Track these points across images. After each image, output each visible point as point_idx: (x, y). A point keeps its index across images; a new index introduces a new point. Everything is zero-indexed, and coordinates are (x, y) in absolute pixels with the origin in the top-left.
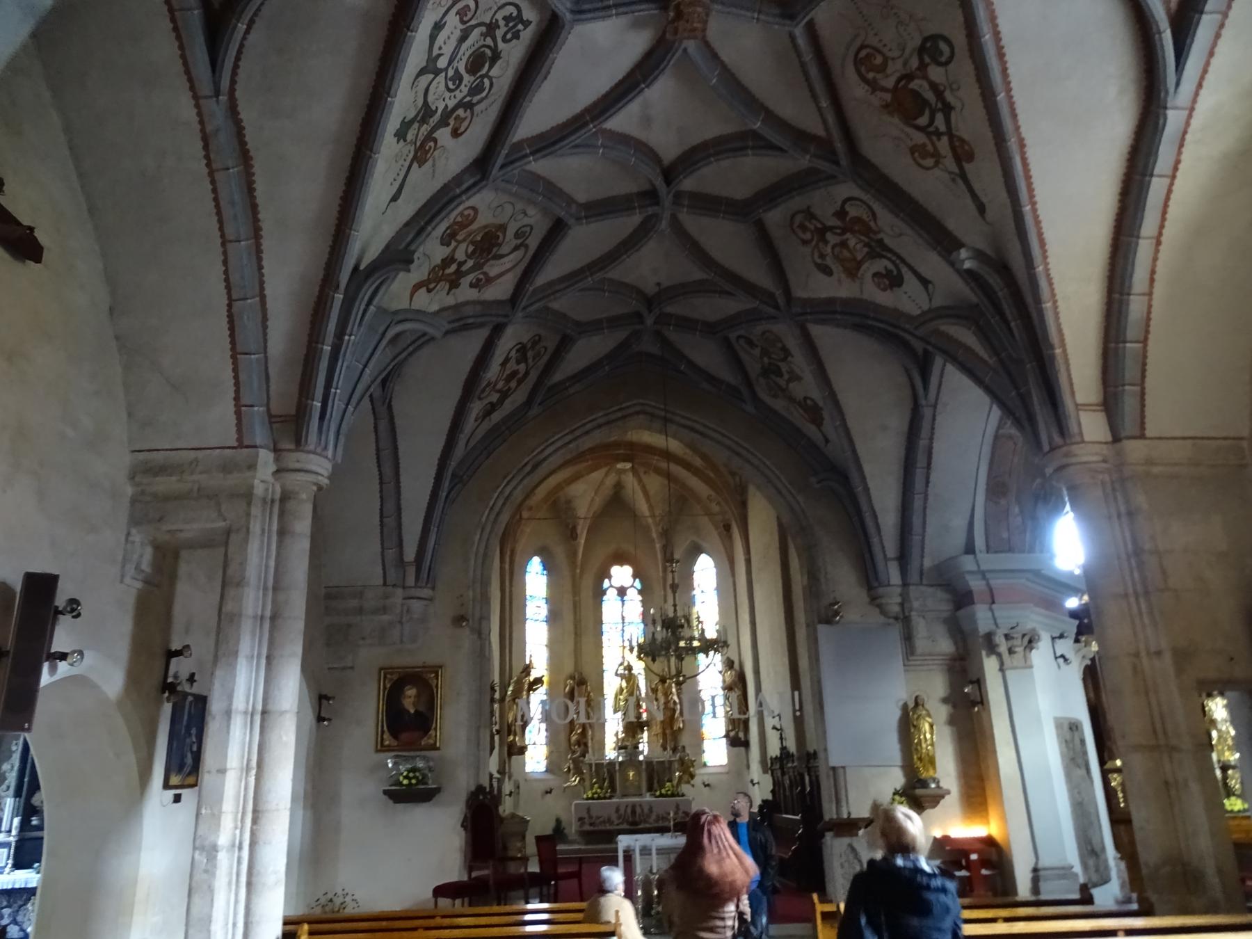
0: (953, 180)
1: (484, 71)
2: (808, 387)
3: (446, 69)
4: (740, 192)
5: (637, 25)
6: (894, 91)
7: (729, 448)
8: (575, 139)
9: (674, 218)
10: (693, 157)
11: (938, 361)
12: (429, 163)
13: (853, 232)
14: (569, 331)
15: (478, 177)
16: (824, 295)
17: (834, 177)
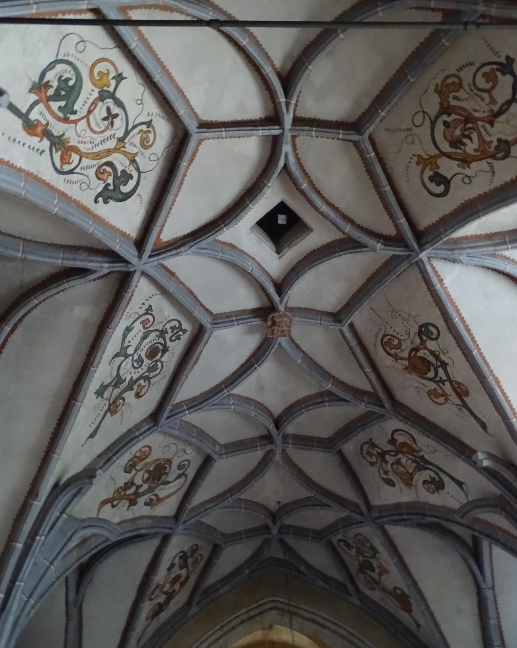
0: (460, 410)
1: (158, 358)
2: (394, 579)
3: (133, 355)
4: (325, 433)
5: (251, 331)
6: (409, 358)
7: (343, 637)
8: (216, 400)
9: (284, 451)
10: (292, 410)
11: (485, 544)
12: (118, 415)
13: (402, 453)
14: (218, 541)
15: (152, 424)
16: (393, 502)
17: (383, 416)
